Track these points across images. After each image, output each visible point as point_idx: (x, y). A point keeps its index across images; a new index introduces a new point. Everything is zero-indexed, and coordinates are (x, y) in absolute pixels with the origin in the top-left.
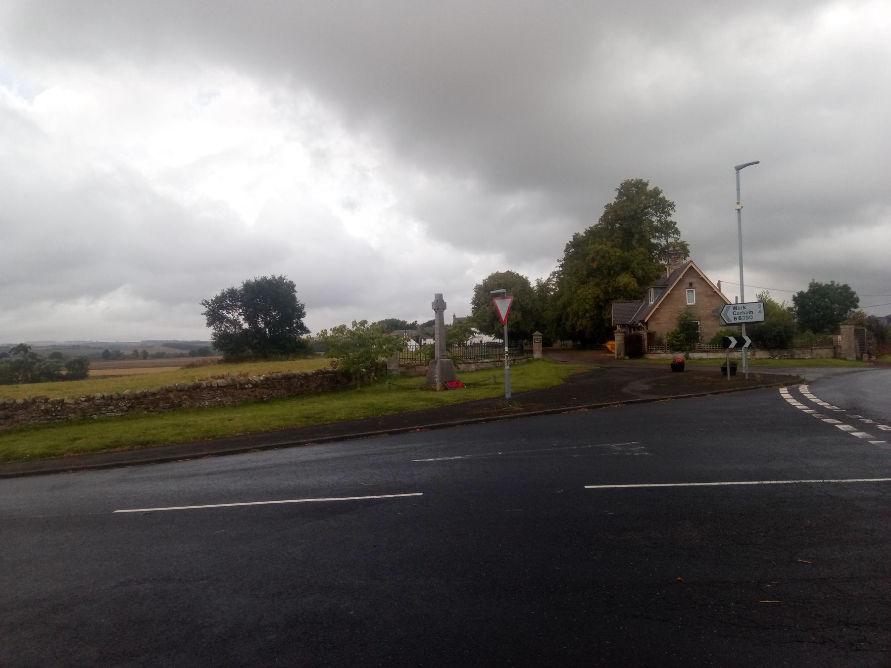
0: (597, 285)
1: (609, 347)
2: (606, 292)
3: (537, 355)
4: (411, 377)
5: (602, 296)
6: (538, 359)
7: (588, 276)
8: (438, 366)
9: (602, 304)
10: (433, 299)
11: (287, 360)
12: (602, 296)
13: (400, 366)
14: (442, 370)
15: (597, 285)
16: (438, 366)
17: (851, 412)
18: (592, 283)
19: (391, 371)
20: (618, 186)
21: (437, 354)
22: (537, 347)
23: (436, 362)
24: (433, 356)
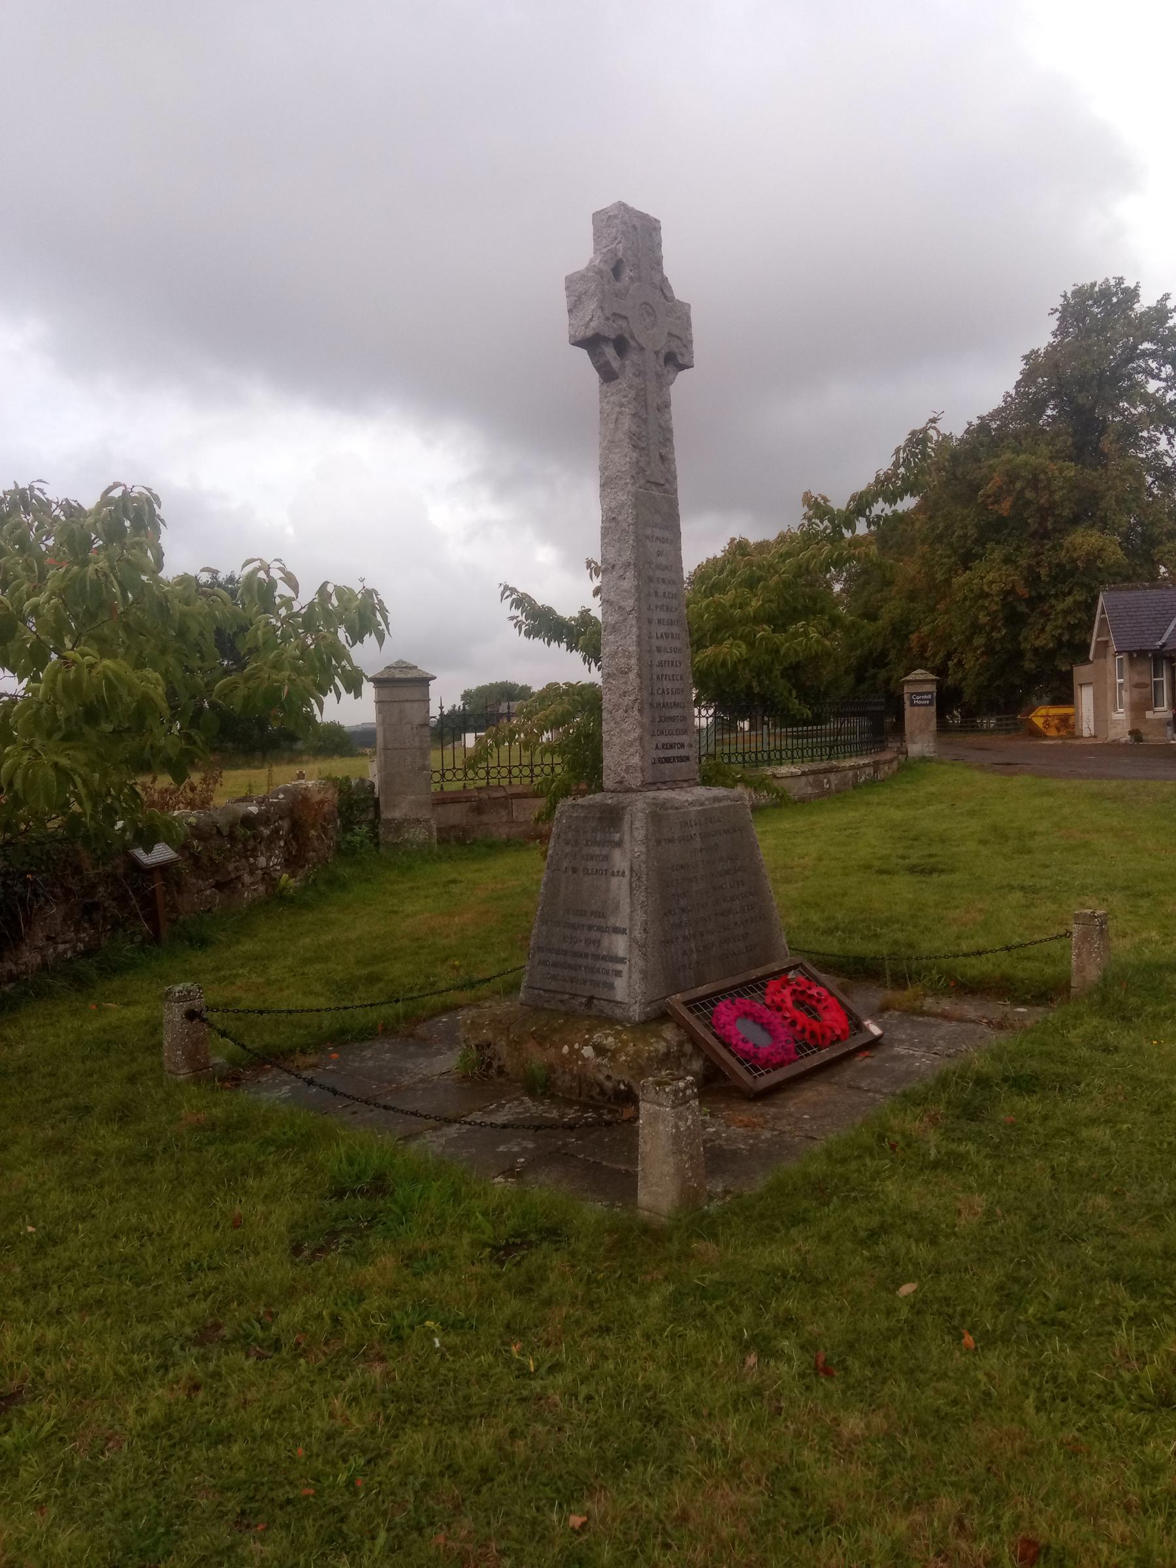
0: (1007, 560)
1: (1039, 722)
2: (1032, 579)
3: (920, 742)
4: (494, 848)
5: (1023, 591)
6: (924, 759)
7: (981, 541)
8: (629, 852)
9: (1022, 608)
10: (580, 252)
11: (248, 765)
12: (1023, 591)
13: (443, 800)
14: (668, 890)
15: (1007, 560)
16: (629, 852)
17: (774, 776)
18: (997, 555)
19: (398, 827)
20: (1058, 303)
21: (623, 748)
22: (919, 717)
23: (611, 817)
24: (585, 759)
